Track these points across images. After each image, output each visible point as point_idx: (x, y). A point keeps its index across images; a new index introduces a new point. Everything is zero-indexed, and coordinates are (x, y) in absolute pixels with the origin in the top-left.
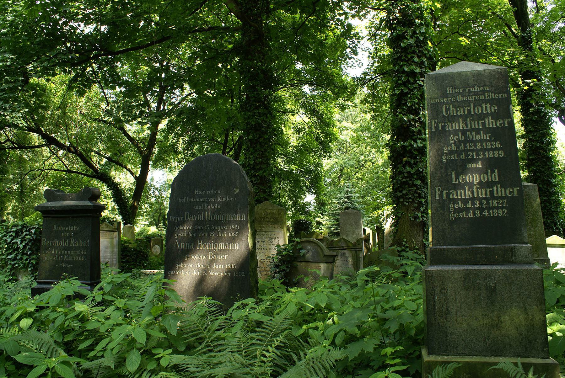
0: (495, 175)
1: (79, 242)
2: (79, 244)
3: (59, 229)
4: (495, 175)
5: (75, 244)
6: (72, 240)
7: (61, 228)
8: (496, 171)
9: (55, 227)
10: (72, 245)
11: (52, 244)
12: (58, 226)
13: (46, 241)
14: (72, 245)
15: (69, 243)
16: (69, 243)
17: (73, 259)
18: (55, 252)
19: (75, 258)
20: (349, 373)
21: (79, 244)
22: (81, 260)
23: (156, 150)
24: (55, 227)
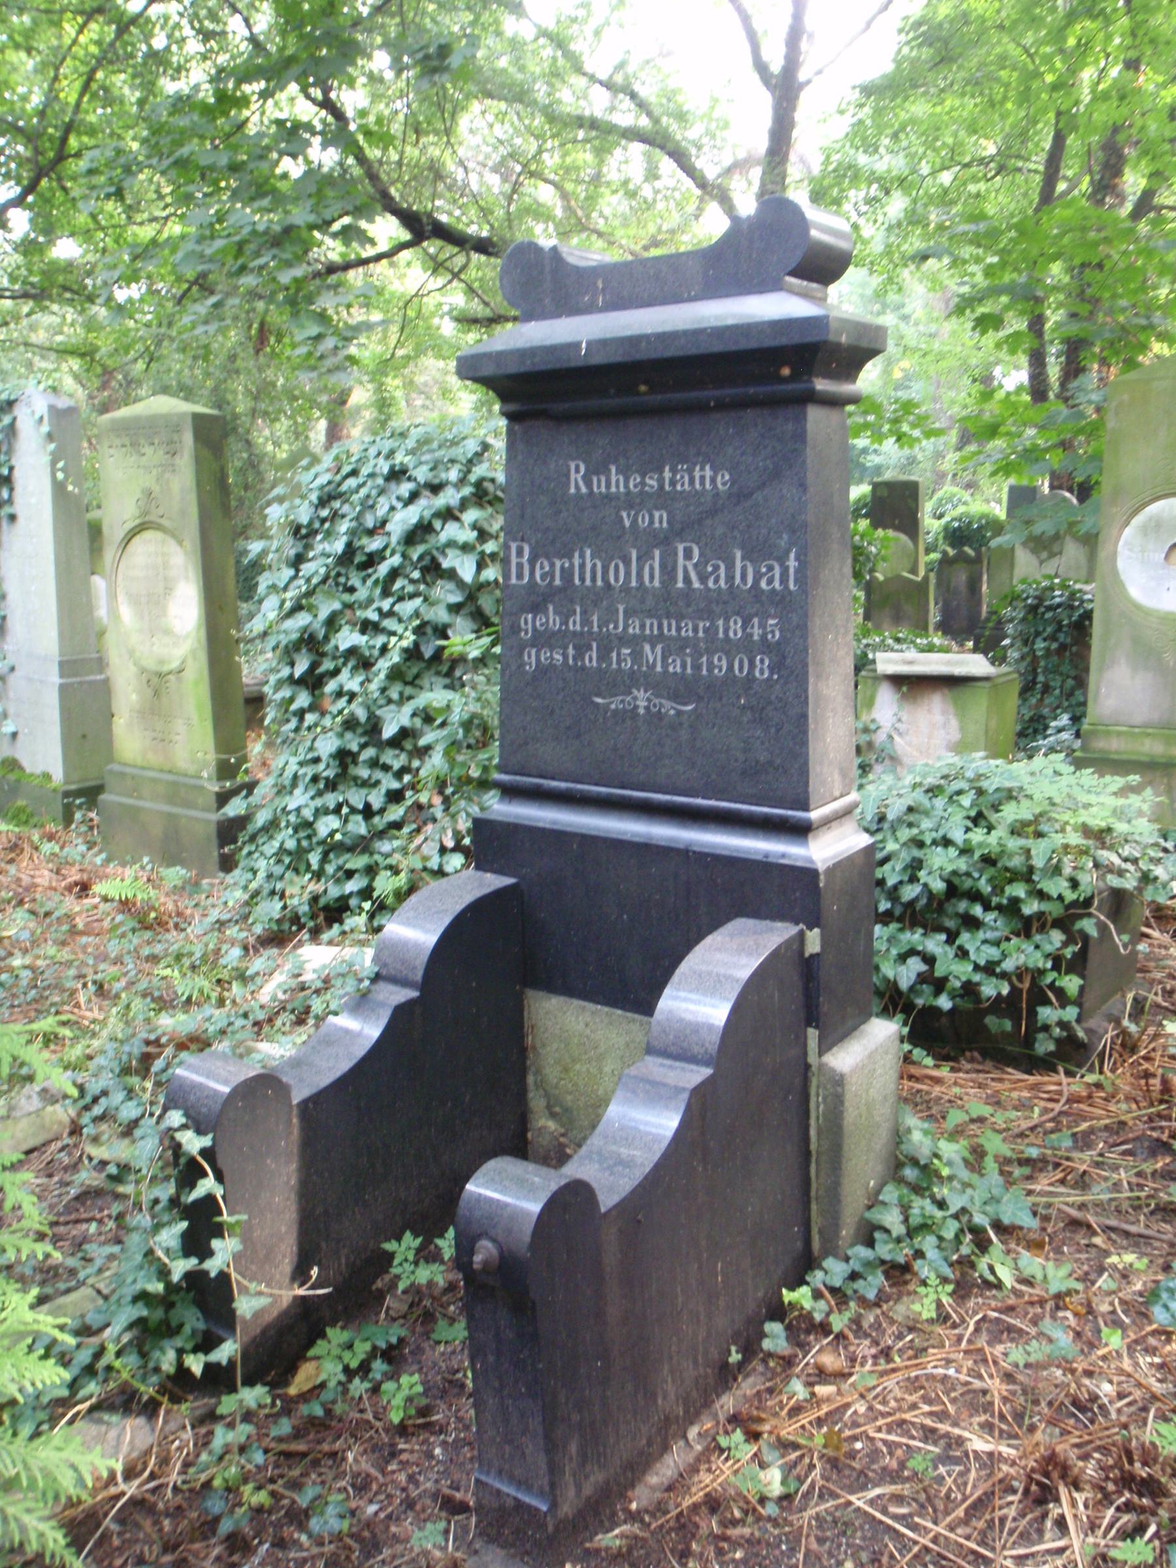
0: (652, 569)
1: (730, 567)
2: (730, 578)
3: (599, 486)
4: (652, 569)
5: (703, 579)
6: (688, 555)
7: (615, 482)
8: (657, 553)
9: (576, 477)
10: (687, 579)
11: (567, 574)
12: (597, 469)
13: (532, 562)
14: (687, 579)
15: (669, 571)
16: (669, 571)
17: (697, 667)
18: (586, 621)
19: (711, 666)
20: (79, 793)
21: (730, 578)
22: (750, 678)
23: (580, 213)
24: (576, 477)
